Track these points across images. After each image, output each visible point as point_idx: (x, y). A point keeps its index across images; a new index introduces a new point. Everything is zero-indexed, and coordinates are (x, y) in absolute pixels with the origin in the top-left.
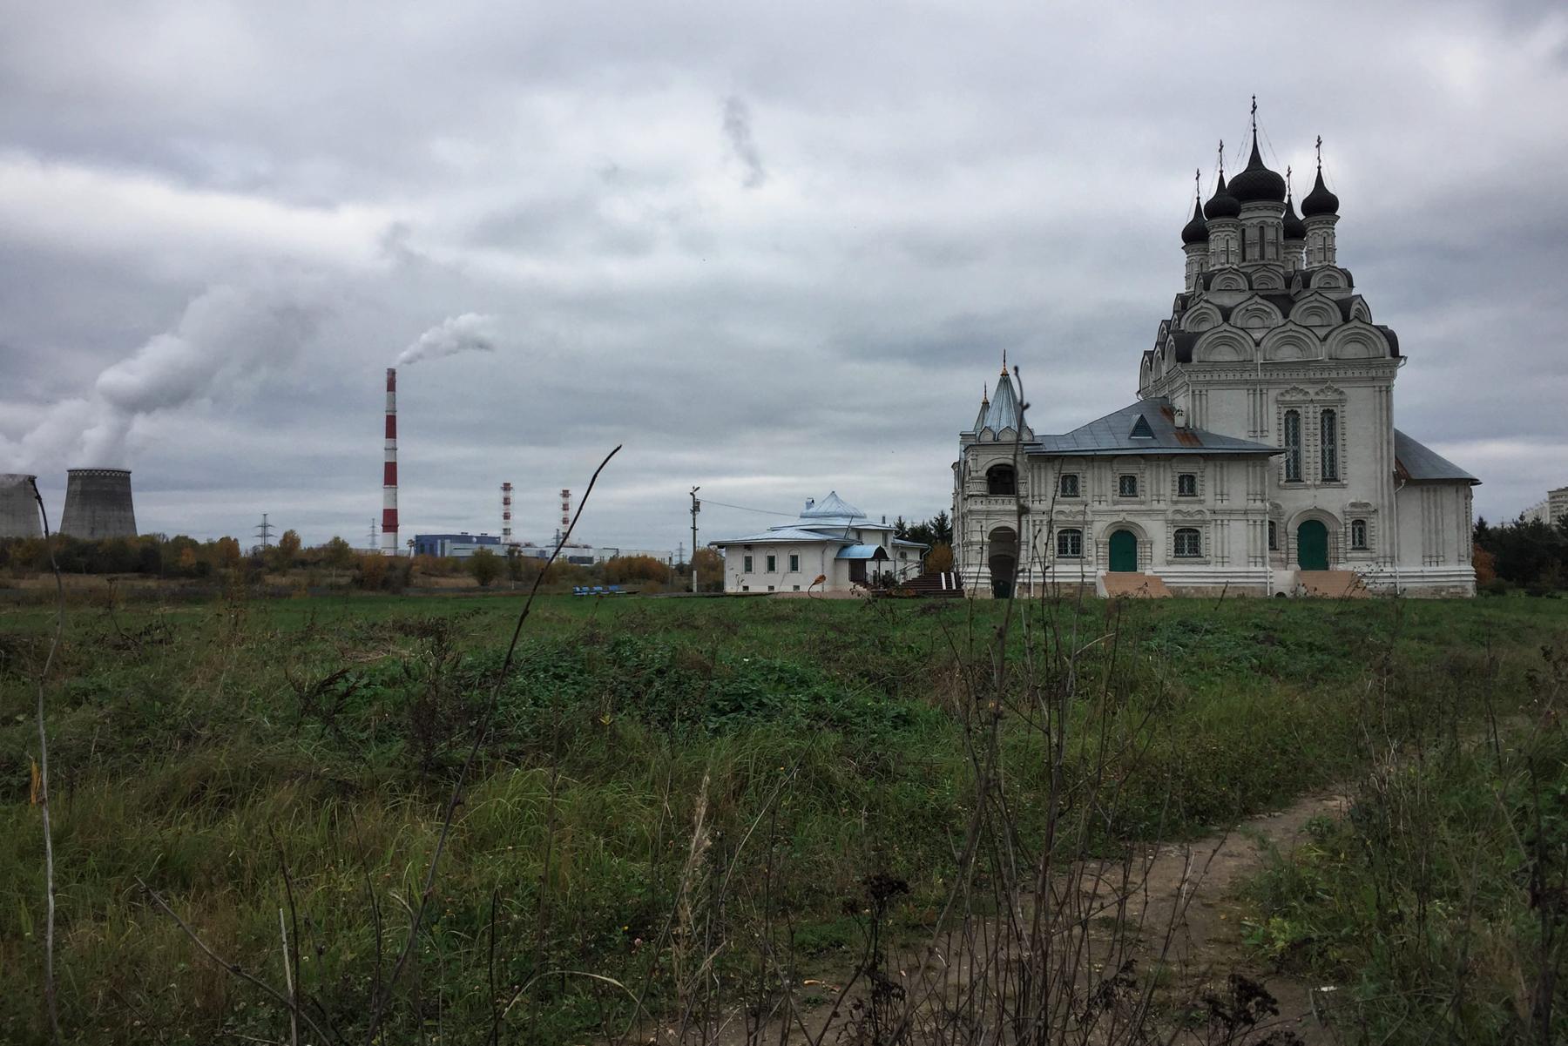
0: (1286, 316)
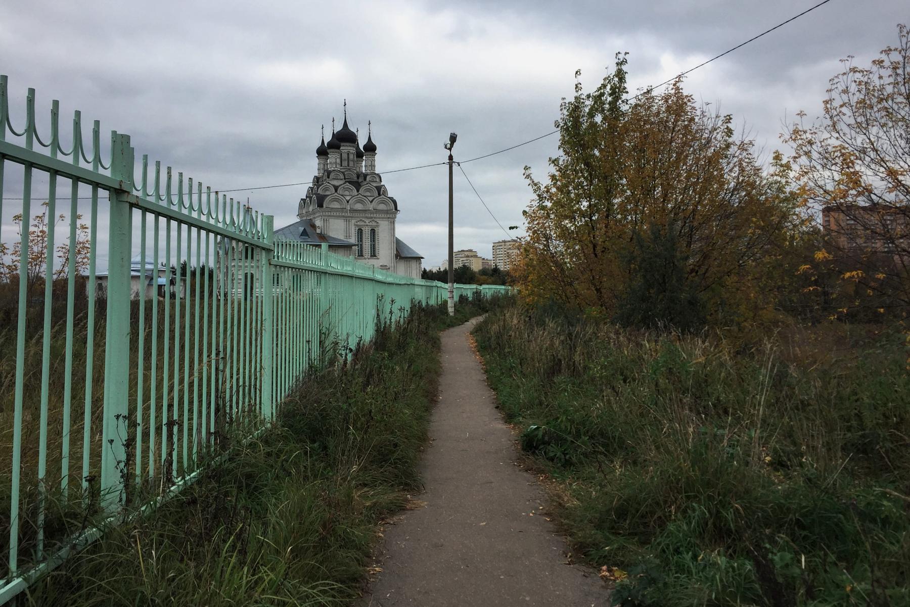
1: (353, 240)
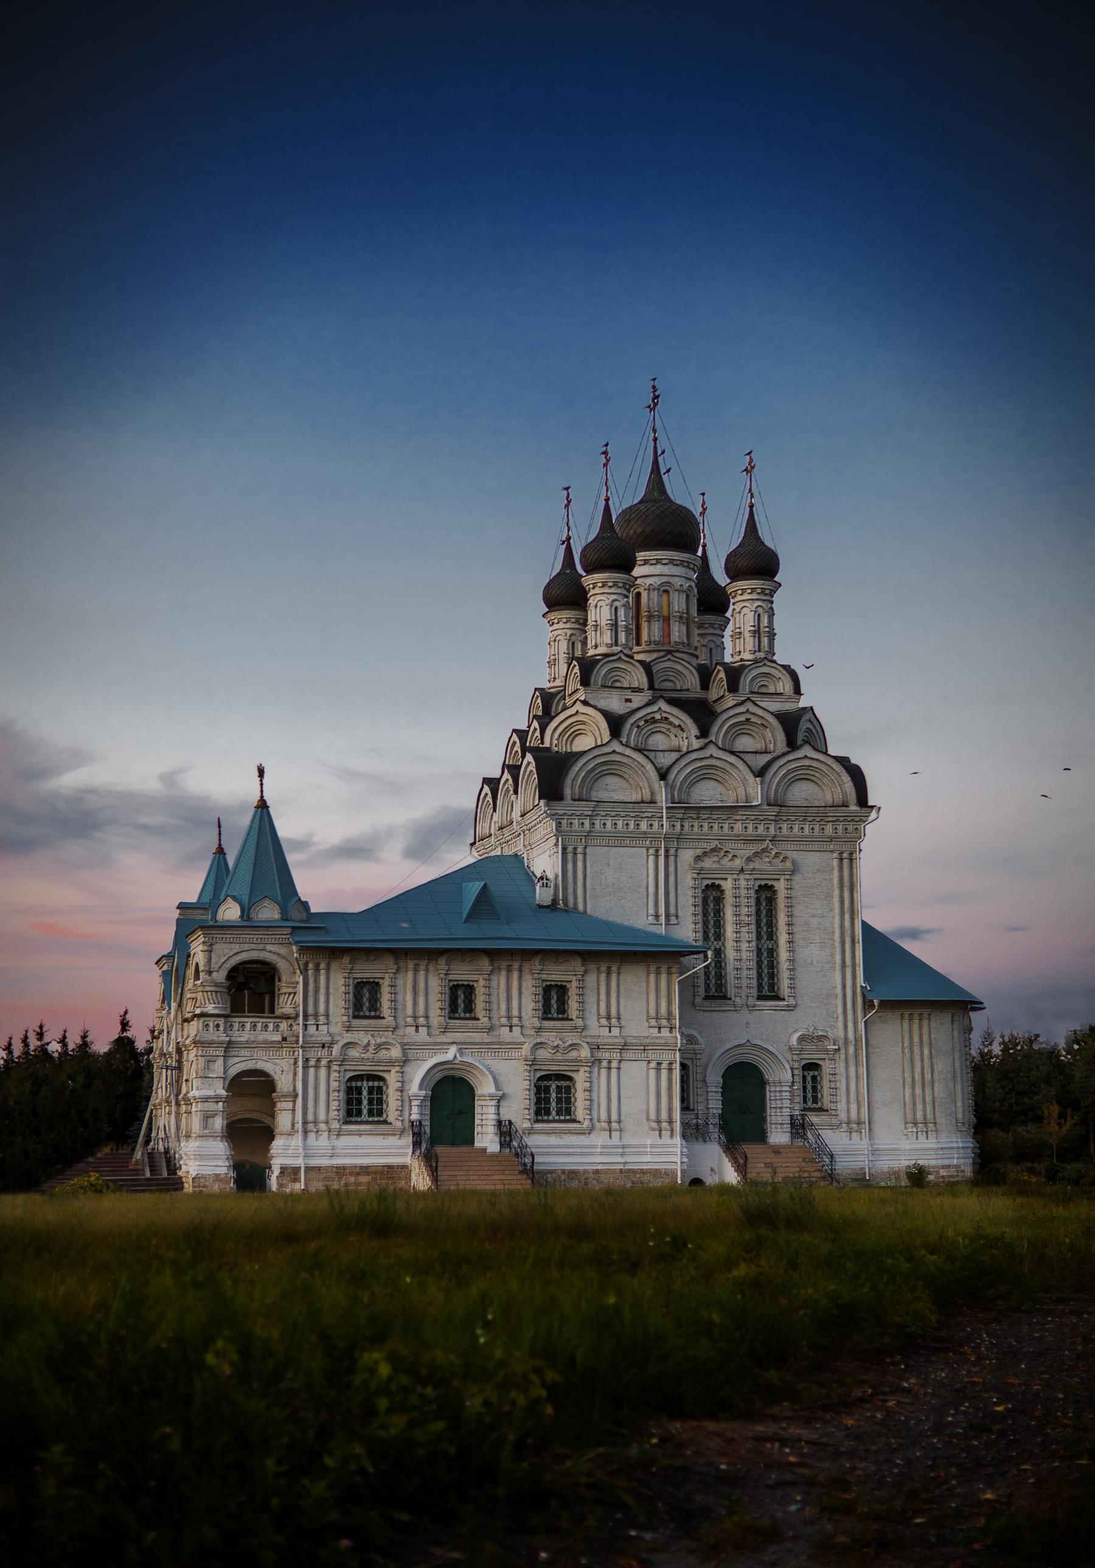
0: (704, 733)
1: (687, 931)
